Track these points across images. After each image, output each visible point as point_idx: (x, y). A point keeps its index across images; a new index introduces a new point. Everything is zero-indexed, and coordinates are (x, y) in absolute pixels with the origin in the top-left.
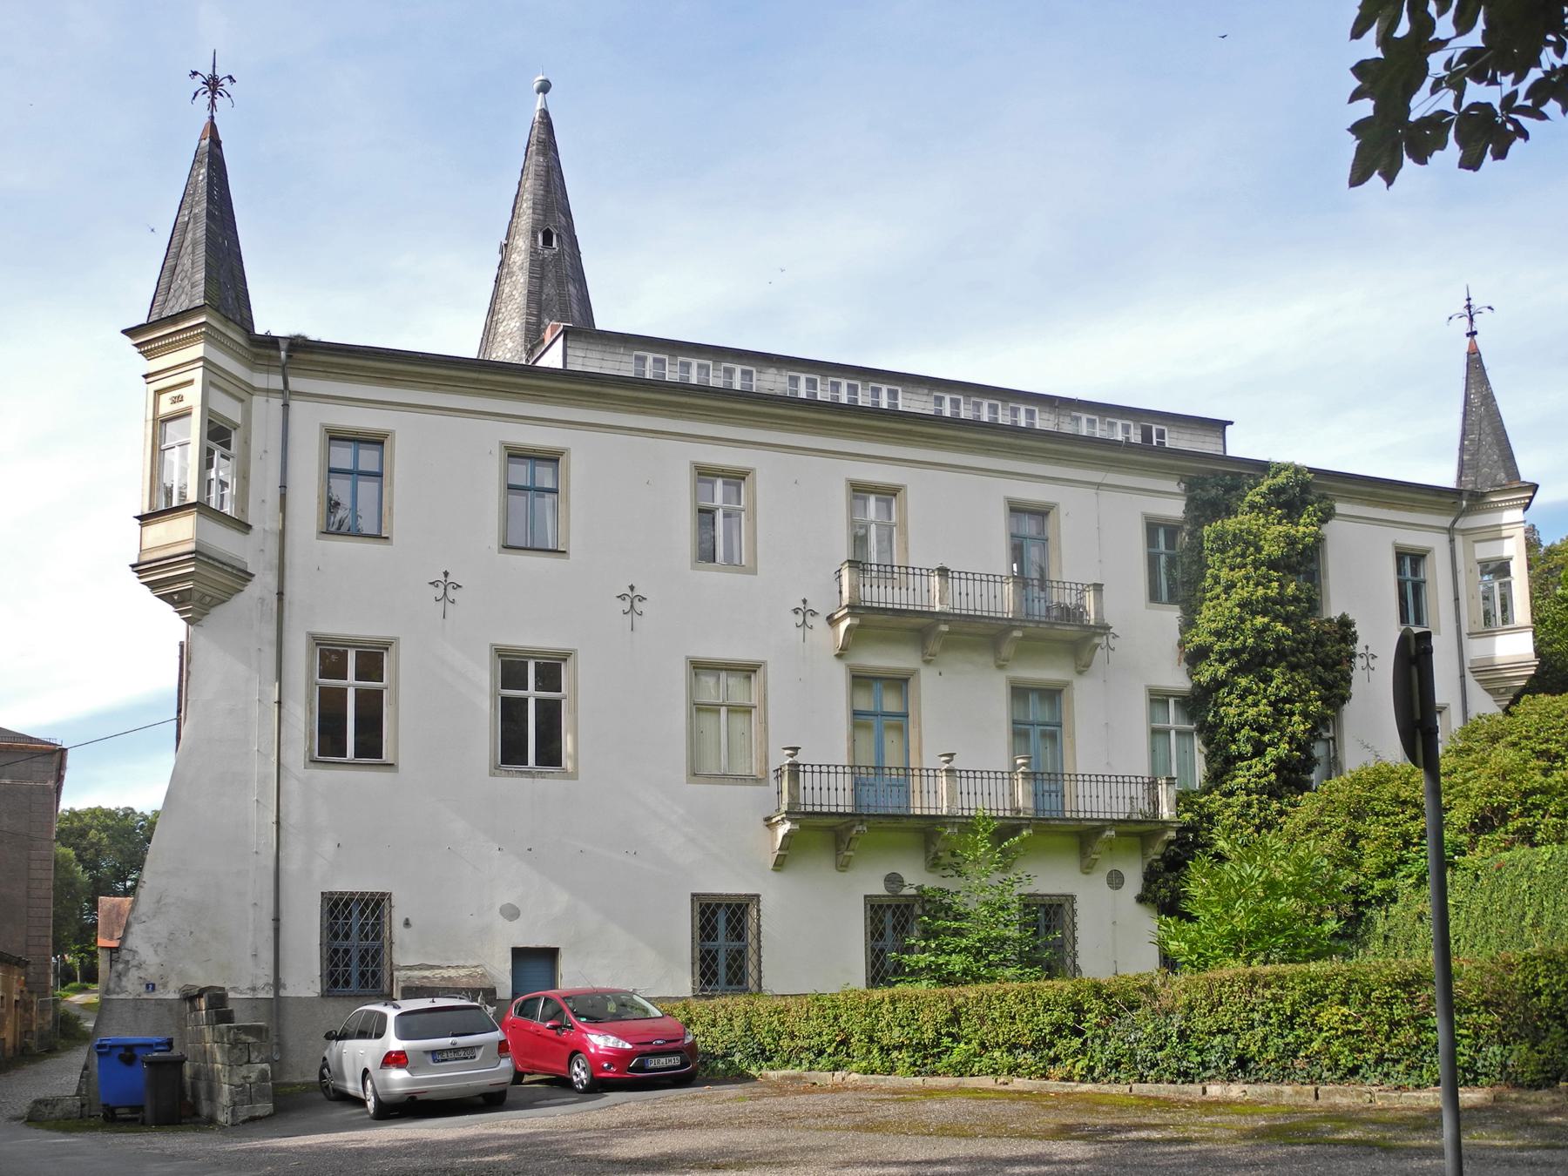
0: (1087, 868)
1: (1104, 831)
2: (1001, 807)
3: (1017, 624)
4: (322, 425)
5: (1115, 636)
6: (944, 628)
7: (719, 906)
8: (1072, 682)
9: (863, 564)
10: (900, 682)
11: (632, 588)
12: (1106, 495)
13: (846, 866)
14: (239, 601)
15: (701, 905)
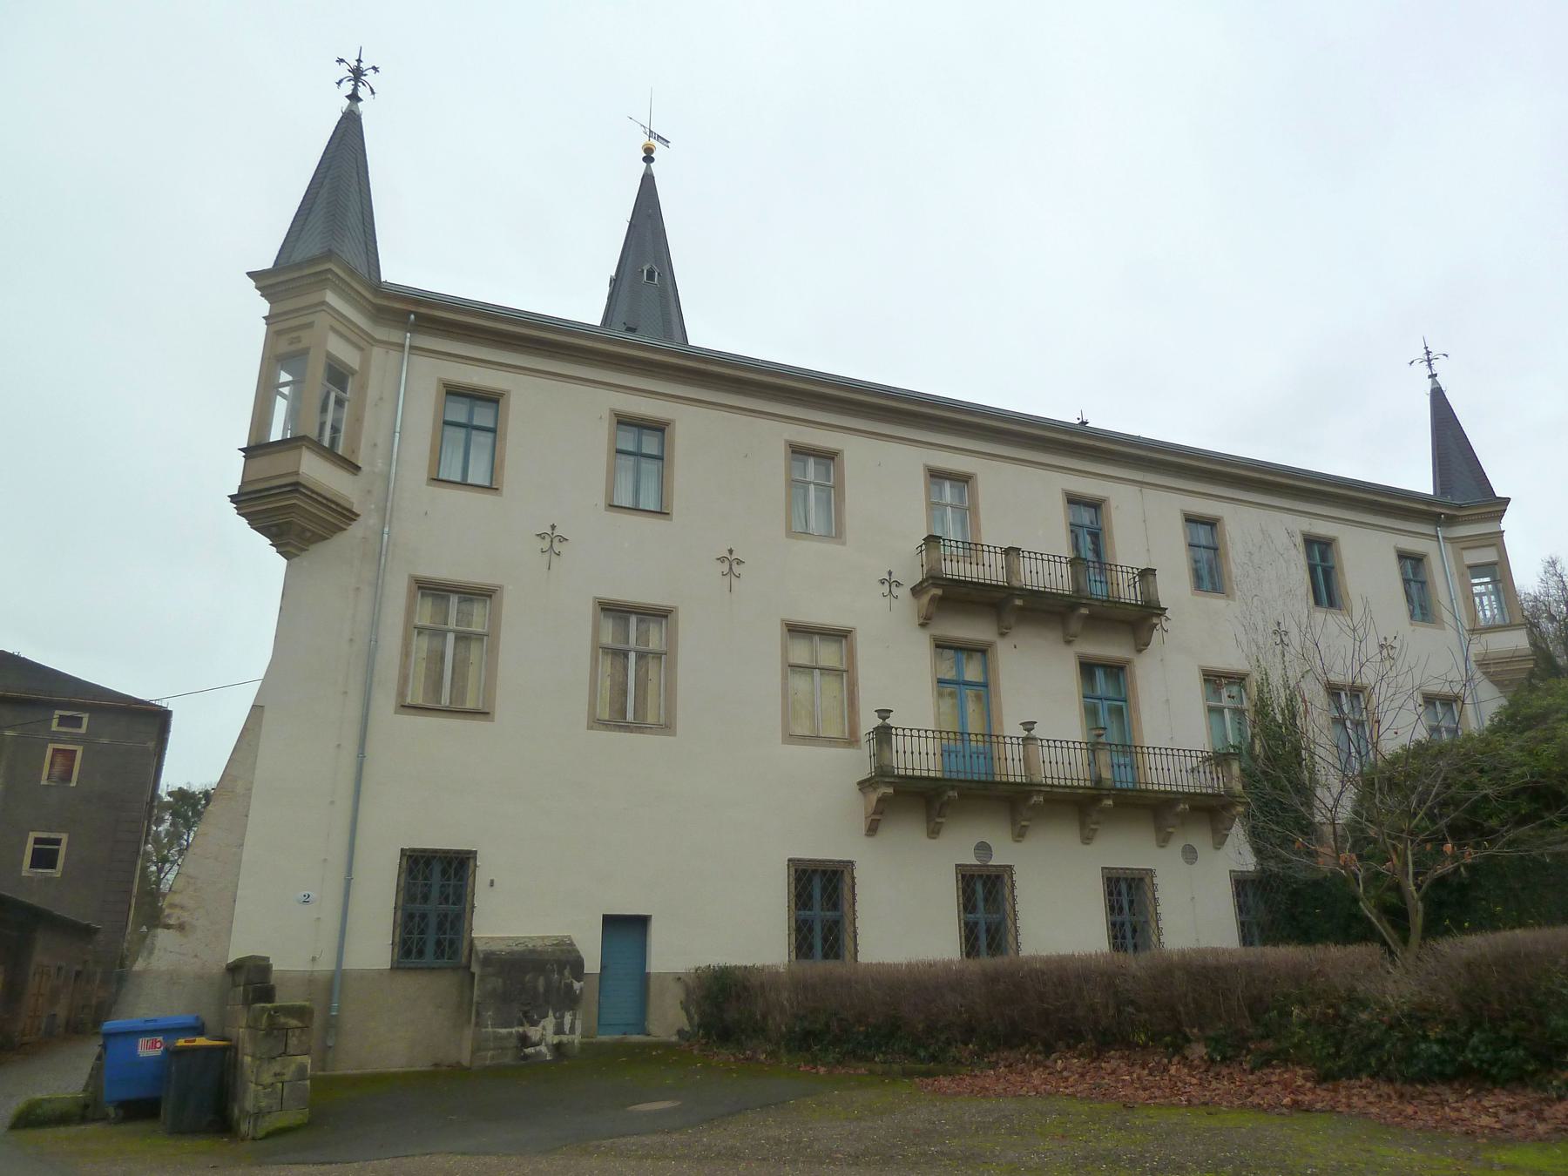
0: (1163, 841)
1: (1031, 797)
2: (1167, 782)
3: (1084, 601)
4: (440, 380)
5: (1167, 619)
6: (1019, 602)
7: (815, 871)
8: (995, 642)
9: (944, 540)
10: (981, 651)
11: (731, 551)
12: (1146, 491)
13: (938, 833)
14: (340, 540)
15: (796, 871)
